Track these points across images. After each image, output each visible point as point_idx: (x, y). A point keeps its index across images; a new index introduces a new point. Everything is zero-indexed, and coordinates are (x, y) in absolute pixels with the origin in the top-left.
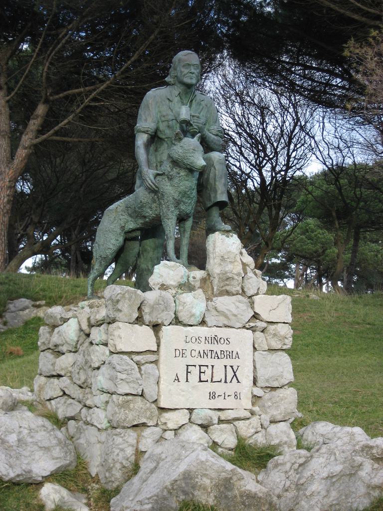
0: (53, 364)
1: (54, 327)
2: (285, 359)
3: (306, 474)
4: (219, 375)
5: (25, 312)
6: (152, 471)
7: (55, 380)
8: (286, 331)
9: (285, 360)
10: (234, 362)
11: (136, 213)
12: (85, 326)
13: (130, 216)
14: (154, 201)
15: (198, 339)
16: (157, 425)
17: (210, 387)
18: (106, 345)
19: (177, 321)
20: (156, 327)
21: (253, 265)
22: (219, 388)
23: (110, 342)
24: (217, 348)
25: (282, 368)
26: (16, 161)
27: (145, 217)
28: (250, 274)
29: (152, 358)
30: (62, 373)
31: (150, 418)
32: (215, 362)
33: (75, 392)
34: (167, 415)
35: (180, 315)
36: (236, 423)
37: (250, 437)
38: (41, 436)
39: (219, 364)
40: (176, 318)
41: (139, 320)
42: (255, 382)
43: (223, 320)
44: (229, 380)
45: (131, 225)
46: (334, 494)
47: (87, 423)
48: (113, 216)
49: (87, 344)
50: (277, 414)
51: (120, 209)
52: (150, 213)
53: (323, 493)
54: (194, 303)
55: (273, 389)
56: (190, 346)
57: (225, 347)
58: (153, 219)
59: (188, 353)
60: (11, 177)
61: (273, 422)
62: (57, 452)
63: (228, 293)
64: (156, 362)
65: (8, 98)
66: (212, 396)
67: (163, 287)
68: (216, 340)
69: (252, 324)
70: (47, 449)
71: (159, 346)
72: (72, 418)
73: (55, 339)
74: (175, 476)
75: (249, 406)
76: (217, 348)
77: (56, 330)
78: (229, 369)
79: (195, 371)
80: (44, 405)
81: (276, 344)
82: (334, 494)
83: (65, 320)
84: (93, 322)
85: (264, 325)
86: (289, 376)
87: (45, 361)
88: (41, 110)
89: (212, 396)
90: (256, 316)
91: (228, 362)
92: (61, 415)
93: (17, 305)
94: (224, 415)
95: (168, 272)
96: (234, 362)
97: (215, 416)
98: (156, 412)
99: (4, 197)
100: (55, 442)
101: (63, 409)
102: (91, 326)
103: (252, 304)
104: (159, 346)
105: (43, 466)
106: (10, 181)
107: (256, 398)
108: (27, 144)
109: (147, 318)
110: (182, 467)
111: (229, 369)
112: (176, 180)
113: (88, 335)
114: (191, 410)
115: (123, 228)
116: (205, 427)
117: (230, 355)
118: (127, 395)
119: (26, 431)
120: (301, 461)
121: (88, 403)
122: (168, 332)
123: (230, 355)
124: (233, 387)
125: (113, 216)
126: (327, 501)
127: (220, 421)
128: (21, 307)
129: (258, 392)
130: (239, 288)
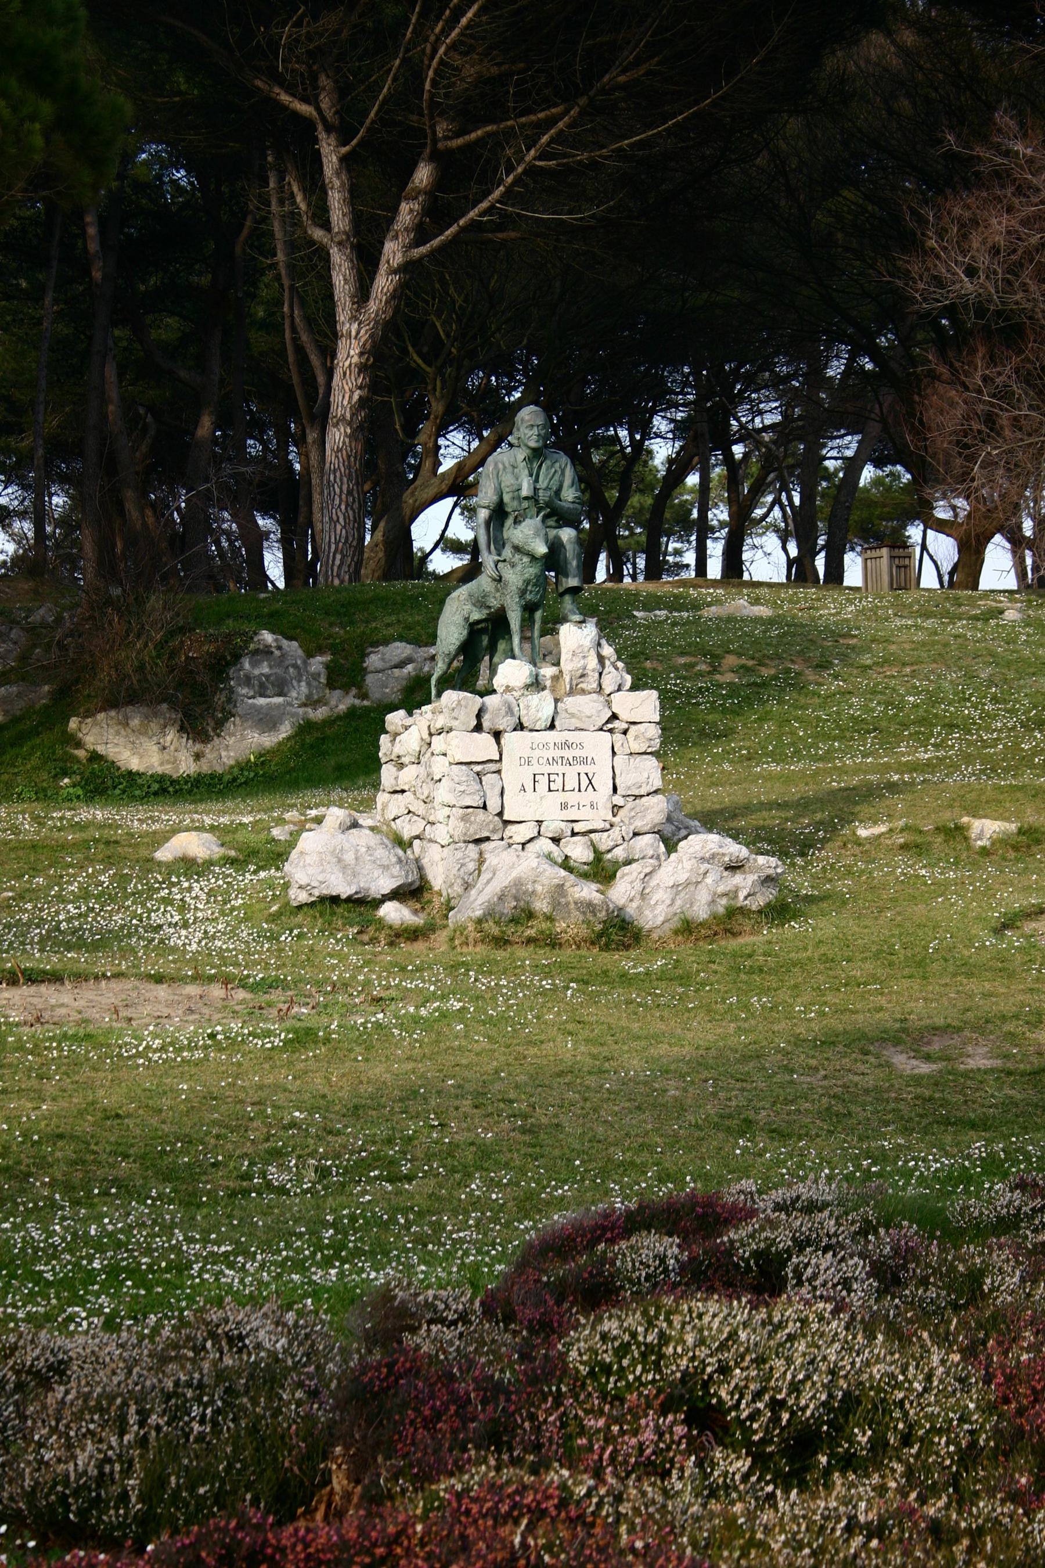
0: (396, 778)
1: (397, 734)
2: (652, 763)
3: (653, 883)
4: (571, 783)
5: (405, 671)
6: (488, 882)
7: (399, 796)
8: (654, 731)
9: (652, 765)
10: (590, 769)
11: (480, 602)
12: (426, 736)
13: (474, 605)
14: (497, 590)
15: (545, 745)
16: (502, 839)
17: (561, 797)
18: (445, 755)
19: (520, 727)
20: (497, 735)
21: (614, 657)
22: (572, 798)
23: (449, 752)
24: (568, 754)
25: (650, 772)
26: (373, 306)
27: (490, 607)
28: (609, 668)
29: (493, 767)
30: (406, 788)
31: (494, 831)
32: (567, 769)
33: (418, 807)
34: (511, 829)
35: (524, 720)
36: (592, 835)
37: (609, 851)
38: (380, 853)
39: (571, 772)
40: (521, 724)
41: (478, 728)
42: (615, 790)
43: (575, 723)
44: (583, 788)
45: (476, 616)
46: (679, 902)
47: (431, 841)
48: (455, 605)
49: (428, 754)
50: (639, 824)
51: (462, 598)
52: (494, 603)
53: (668, 902)
54: (539, 707)
55: (637, 797)
56: (537, 753)
57: (577, 753)
58: (499, 609)
59: (534, 761)
60: (364, 345)
61: (636, 834)
62: (396, 870)
63: (583, 692)
64: (499, 772)
65: (344, 150)
66: (564, 806)
67: (508, 689)
68: (567, 745)
69: (610, 726)
70: (385, 868)
71: (501, 755)
72: (418, 837)
73: (398, 749)
74: (506, 883)
75: (610, 817)
76: (568, 754)
77: (398, 739)
78: (583, 777)
79: (543, 781)
80: (388, 825)
81: (636, 747)
82: (679, 902)
83: (407, 728)
84: (433, 731)
85: (626, 726)
86: (657, 783)
87: (388, 774)
88: (423, 175)
89: (564, 806)
90: (614, 717)
91: (582, 769)
92: (406, 836)
93: (387, 656)
94: (578, 827)
95: (511, 672)
96: (590, 769)
97: (567, 829)
98: (501, 825)
99: (352, 392)
100: (394, 860)
101: (407, 829)
102: (431, 735)
103: (609, 704)
104: (501, 755)
105: (385, 884)
106: (361, 354)
107: (616, 809)
108: (397, 260)
109: (486, 724)
110: (514, 874)
111: (583, 777)
112: (519, 568)
113: (430, 744)
114: (540, 822)
115: (467, 619)
116: (556, 840)
117: (584, 761)
118: (468, 807)
119: (364, 850)
120: (648, 870)
121: (431, 819)
122: (507, 739)
123: (584, 761)
124: (589, 796)
125: (455, 605)
126: (672, 910)
127: (574, 834)
128: (396, 660)
129: (618, 800)
130: (595, 685)
